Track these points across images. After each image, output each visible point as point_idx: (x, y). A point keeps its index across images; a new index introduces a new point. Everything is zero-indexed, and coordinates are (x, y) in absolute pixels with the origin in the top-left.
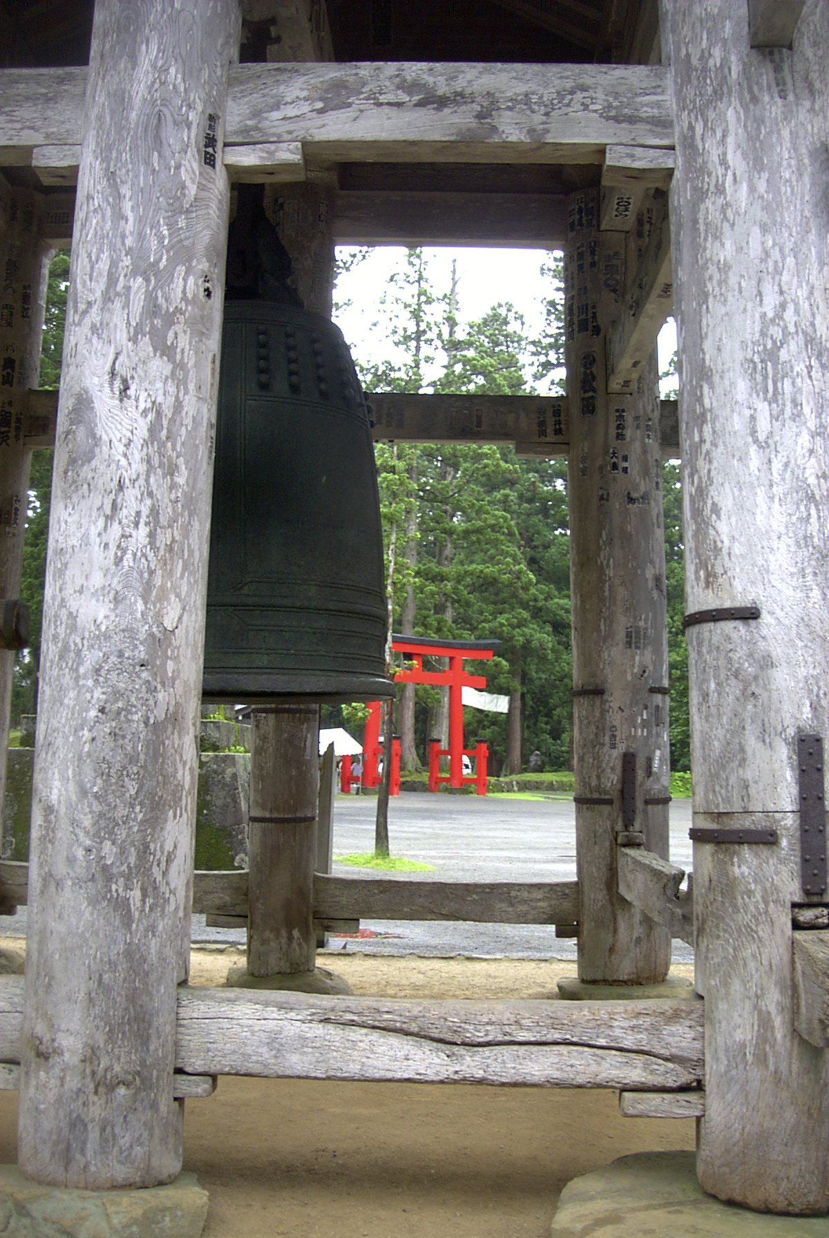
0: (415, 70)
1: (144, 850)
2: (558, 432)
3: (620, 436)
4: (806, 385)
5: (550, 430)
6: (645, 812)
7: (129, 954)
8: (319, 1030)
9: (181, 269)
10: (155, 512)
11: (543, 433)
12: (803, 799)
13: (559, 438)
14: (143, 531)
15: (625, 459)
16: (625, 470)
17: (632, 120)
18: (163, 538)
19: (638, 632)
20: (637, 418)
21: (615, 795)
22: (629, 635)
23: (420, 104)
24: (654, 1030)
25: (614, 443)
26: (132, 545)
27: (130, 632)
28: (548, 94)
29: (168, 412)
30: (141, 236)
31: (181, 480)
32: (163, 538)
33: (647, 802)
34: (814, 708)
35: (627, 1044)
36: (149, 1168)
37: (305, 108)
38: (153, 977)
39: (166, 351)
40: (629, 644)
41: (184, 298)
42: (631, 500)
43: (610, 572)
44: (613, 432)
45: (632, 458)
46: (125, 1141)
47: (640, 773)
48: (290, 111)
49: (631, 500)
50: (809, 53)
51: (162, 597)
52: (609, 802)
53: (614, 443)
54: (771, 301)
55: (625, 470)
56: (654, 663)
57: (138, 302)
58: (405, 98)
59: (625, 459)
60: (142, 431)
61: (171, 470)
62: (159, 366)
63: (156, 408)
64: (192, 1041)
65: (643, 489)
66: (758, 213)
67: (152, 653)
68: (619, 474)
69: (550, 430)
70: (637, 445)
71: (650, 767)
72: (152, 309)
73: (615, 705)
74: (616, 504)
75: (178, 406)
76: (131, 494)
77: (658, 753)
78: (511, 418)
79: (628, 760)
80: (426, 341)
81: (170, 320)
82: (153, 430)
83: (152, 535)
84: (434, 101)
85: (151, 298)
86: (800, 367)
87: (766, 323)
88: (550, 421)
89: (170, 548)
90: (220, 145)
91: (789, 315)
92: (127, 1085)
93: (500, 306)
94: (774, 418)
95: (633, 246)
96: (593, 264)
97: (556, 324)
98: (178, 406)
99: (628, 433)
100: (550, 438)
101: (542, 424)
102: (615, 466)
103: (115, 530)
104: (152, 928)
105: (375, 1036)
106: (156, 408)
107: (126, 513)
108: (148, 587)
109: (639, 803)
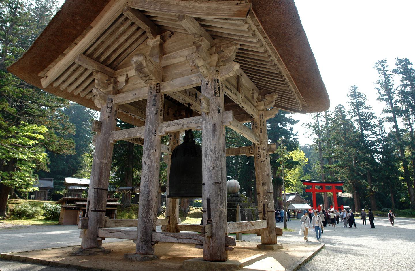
0: (176, 121)
1: (147, 215)
2: (252, 152)
3: (259, 152)
4: (210, 155)
5: (250, 152)
6: (267, 214)
7: (145, 227)
8: (165, 236)
9: (152, 149)
10: (149, 177)
11: (249, 152)
12: (208, 207)
13: (252, 153)
14: (147, 179)
15: (260, 155)
16: (260, 157)
17: (198, 123)
18: (150, 179)
19: (264, 183)
20: (262, 148)
21: (262, 211)
22: (262, 184)
23: (177, 125)
24: (198, 237)
25: (258, 153)
26: (146, 181)
27: (146, 190)
28: (189, 121)
29: (150, 165)
30: (147, 146)
31: (152, 173)
32: (150, 179)
33: (268, 212)
34: (209, 195)
35: (195, 238)
36: (147, 252)
37: (165, 127)
38: (148, 229)
39: (150, 159)
40: (263, 186)
41: (152, 152)
42: (261, 162)
43: (259, 174)
44: (258, 151)
45: (261, 155)
46: (144, 249)
47: (266, 207)
48: (164, 128)
49: (261, 162)
50: (212, 112)
51: (150, 186)
52: (261, 212)
53: (258, 153)
54: (206, 145)
55: (260, 157)
56: (268, 188)
57: (147, 153)
58: (175, 124)
59: (260, 155)
60: (147, 168)
61: (151, 172)
62: (149, 160)
63: (149, 165)
64: (153, 237)
65: (263, 159)
66: (205, 135)
67: (148, 192)
68: (259, 158)
69: (250, 152)
70: (262, 152)
71: (268, 206)
72: (148, 154)
73: (261, 196)
74: (259, 163)
75: (151, 164)
76: (146, 175)
77: (269, 204)
78: (244, 150)
79: (264, 205)
80: (319, 117)
81: (150, 155)
82: (148, 168)
83: (148, 179)
84: (178, 124)
85: (148, 153)
86: (209, 153)
87: (206, 148)
88: (250, 150)
89: (150, 181)
90: (157, 133)
91: (208, 147)
92: (144, 242)
93: (338, 105)
94: (206, 160)
95: (259, 120)
96: (253, 124)
97: (353, 107)
98: (151, 164)
99: (260, 151)
100: (251, 153)
101: (249, 151)
102: (258, 157)
103: (145, 179)
104: (148, 224)
105: (170, 237)
106: (149, 165)
107: (146, 177)
108: (148, 185)
109: (266, 212)
